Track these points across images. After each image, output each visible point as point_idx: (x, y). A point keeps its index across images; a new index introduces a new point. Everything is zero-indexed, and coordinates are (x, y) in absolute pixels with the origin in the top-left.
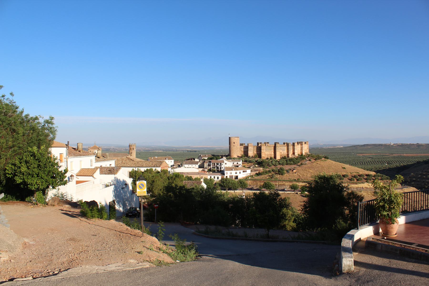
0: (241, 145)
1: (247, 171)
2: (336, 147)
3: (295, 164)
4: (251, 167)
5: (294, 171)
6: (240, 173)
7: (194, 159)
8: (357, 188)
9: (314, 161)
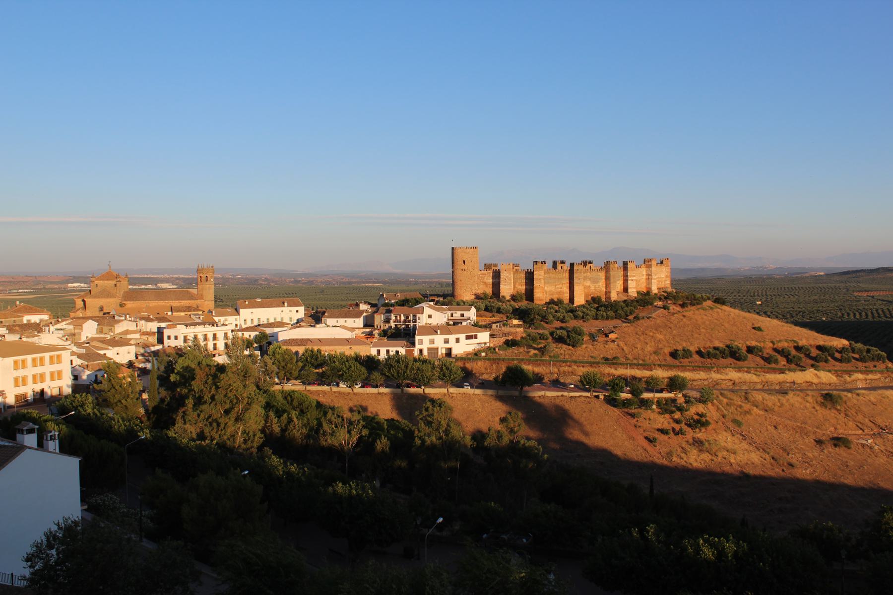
0: (487, 267)
1: (479, 335)
2: (807, 275)
3: (617, 317)
4: (494, 326)
5: (612, 336)
6: (458, 340)
7: (357, 305)
8: (780, 383)
9: (678, 309)
